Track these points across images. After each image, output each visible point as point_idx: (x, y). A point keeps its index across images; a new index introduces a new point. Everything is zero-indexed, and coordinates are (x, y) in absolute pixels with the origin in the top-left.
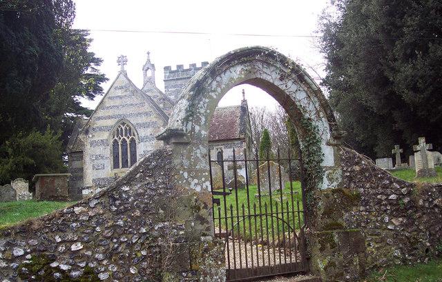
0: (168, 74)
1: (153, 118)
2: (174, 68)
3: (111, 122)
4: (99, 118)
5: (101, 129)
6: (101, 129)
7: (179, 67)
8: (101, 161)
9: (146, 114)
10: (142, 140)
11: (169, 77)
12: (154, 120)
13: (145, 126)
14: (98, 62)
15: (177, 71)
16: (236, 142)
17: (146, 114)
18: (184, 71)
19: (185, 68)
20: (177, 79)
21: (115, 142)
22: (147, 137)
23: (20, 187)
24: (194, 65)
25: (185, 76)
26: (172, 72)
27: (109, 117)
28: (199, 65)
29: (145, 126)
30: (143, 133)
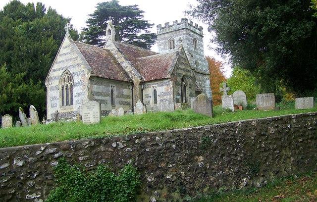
0: (159, 30)
1: (82, 68)
2: (163, 26)
3: (60, 73)
4: (55, 71)
5: (55, 78)
6: (55, 78)
7: (166, 24)
8: (55, 101)
9: (78, 65)
10: (52, 89)
11: (160, 32)
12: (82, 69)
13: (77, 74)
14: (69, 20)
15: (165, 27)
16: (166, 81)
17: (78, 65)
18: (169, 27)
19: (170, 25)
20: (165, 33)
21: (63, 87)
22: (78, 83)
23: (7, 120)
24: (176, 22)
25: (170, 30)
26: (162, 28)
27: (60, 69)
28: (179, 21)
29: (77, 74)
30: (76, 79)
